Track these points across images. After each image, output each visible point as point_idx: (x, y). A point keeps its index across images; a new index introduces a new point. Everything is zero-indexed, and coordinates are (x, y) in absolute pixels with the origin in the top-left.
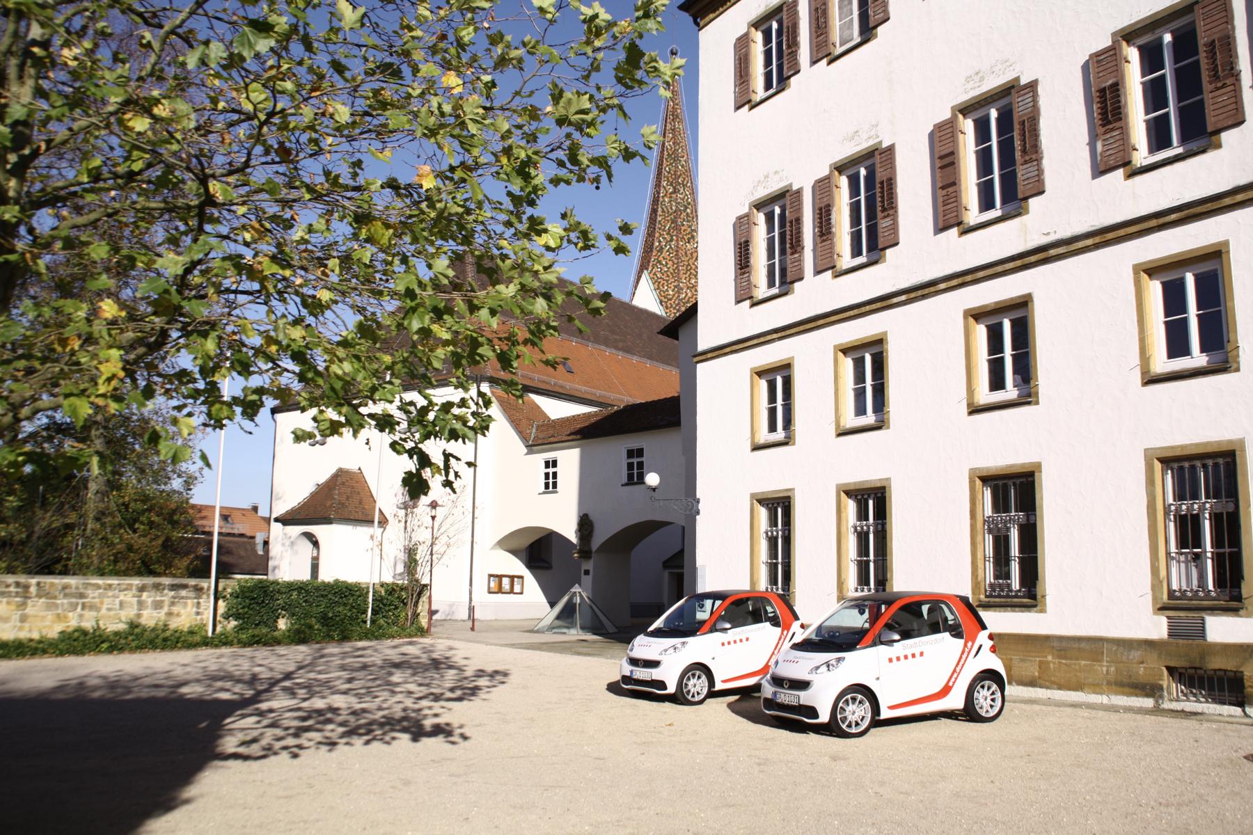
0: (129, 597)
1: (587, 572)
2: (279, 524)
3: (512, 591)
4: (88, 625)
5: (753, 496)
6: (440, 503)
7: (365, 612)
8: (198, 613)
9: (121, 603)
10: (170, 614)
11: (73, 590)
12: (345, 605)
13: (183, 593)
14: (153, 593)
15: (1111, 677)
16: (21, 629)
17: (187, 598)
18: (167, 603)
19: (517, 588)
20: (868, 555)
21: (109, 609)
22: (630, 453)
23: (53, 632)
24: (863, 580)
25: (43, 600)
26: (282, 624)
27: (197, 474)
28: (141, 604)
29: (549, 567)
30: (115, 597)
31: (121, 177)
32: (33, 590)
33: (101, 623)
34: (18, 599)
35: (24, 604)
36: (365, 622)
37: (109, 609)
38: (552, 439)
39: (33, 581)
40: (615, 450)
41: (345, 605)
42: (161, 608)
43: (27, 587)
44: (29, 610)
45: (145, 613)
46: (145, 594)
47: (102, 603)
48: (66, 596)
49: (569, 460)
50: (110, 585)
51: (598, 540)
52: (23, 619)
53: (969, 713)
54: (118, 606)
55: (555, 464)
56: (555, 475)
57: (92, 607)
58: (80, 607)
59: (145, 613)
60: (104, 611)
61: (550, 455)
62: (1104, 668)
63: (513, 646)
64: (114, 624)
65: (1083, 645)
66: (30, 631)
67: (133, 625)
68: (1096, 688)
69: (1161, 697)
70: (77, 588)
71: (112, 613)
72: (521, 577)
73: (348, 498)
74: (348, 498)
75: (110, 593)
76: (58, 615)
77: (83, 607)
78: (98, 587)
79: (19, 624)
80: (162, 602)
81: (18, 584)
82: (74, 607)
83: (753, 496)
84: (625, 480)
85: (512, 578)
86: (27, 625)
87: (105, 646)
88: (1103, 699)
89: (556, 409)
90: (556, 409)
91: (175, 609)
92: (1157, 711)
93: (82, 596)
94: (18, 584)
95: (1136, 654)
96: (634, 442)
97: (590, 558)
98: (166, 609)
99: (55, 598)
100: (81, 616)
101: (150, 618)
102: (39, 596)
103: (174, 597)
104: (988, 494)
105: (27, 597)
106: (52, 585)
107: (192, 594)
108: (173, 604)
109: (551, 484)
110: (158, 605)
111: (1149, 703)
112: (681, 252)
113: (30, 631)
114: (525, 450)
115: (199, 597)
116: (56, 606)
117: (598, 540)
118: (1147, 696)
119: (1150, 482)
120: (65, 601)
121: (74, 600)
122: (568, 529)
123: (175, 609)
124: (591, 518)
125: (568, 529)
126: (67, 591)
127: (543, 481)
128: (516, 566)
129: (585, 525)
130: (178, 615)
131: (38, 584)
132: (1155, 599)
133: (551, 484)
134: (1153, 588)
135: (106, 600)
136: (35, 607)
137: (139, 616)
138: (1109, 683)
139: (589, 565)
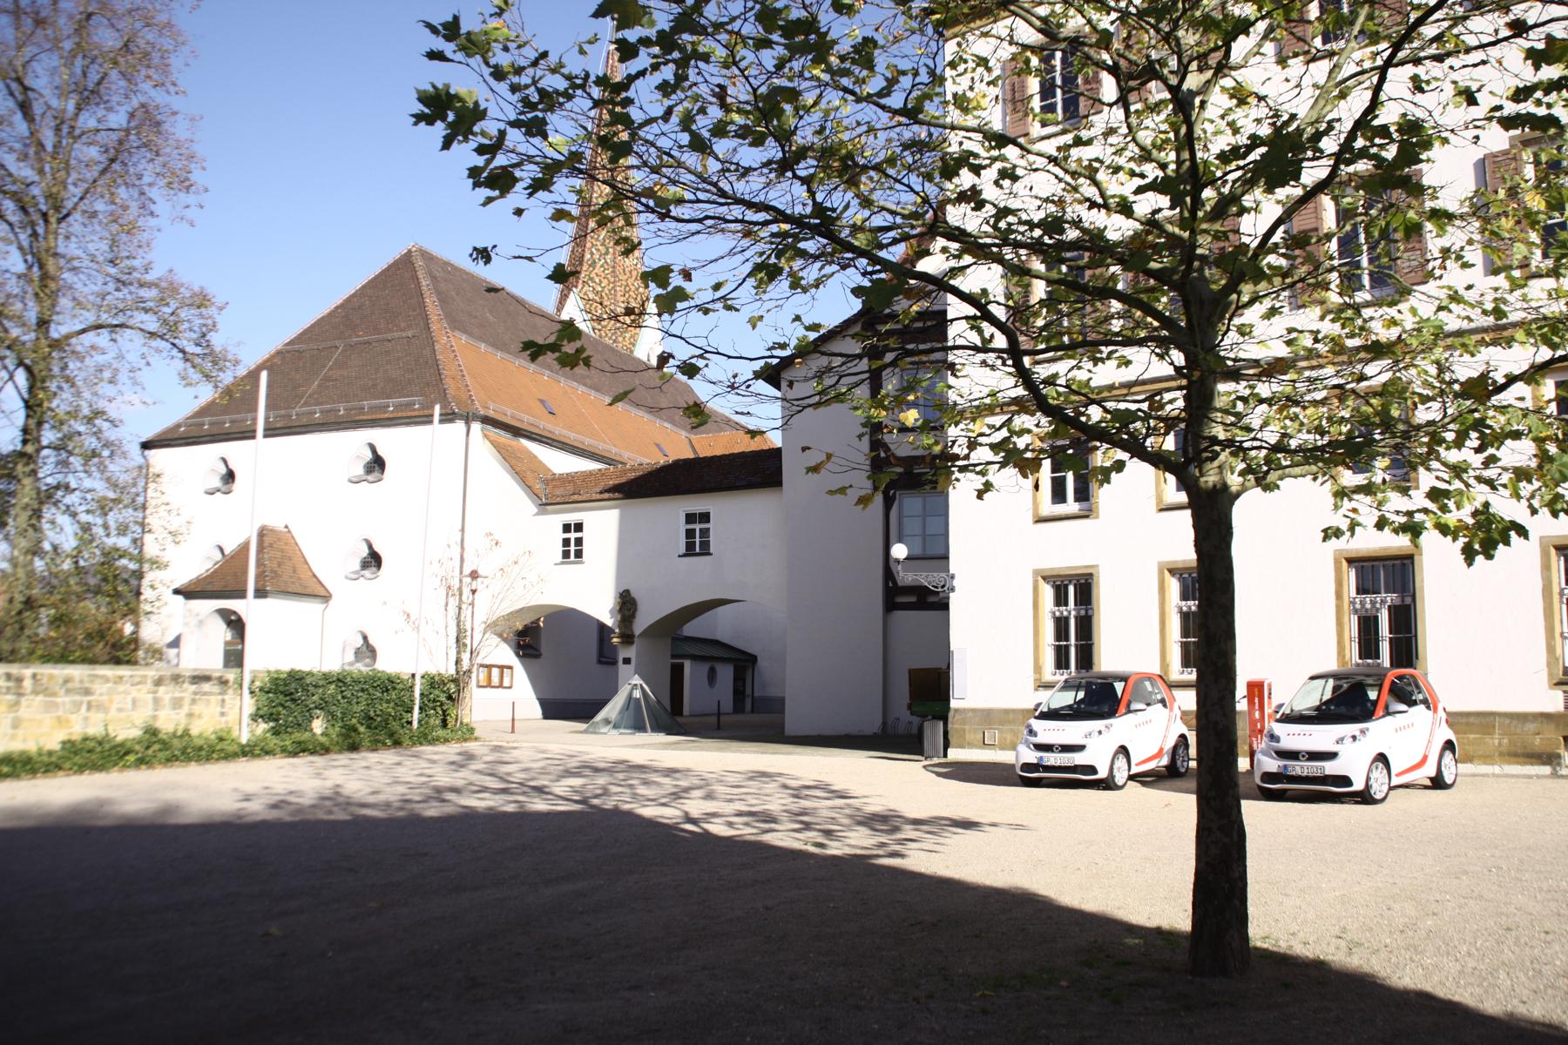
0: (143, 693)
1: (627, 661)
2: (180, 598)
3: (501, 686)
4: (95, 730)
5: (1036, 572)
6: (480, 572)
7: (410, 711)
8: (223, 714)
9: (134, 701)
10: (190, 715)
11: (77, 685)
12: (388, 702)
13: (206, 687)
14: (171, 687)
15: (1504, 749)
16: (13, 737)
17: (210, 694)
18: (187, 701)
19: (506, 683)
20: (1067, 639)
21: (120, 710)
22: (690, 518)
23: (53, 742)
24: (1061, 662)
25: (40, 698)
26: (318, 726)
27: (183, 530)
28: (157, 702)
29: (537, 656)
30: (127, 693)
31: (1038, 226)
32: (28, 684)
33: (110, 729)
34: (9, 697)
35: (17, 703)
36: (410, 723)
37: (120, 710)
38: (576, 497)
39: (27, 672)
40: (670, 514)
41: (388, 702)
42: (180, 707)
43: (19, 680)
44: (23, 712)
45: (162, 714)
46: (162, 689)
47: (111, 701)
48: (68, 691)
49: (603, 525)
50: (121, 678)
51: (645, 619)
52: (16, 724)
53: (1438, 783)
54: (130, 706)
55: (579, 527)
56: (579, 542)
57: (100, 707)
58: (84, 707)
59: (162, 714)
60: (113, 712)
61: (572, 518)
62: (1496, 740)
63: (637, 746)
64: (127, 731)
65: (1472, 720)
66: (24, 740)
67: (152, 732)
68: (1487, 759)
69: (1559, 764)
70: (81, 681)
71: (123, 715)
72: (510, 668)
73: (279, 565)
74: (279, 565)
75: (121, 688)
76: (59, 718)
77: (89, 707)
78: (106, 679)
79: (10, 731)
80: (181, 699)
81: (9, 677)
82: (77, 706)
83: (1036, 572)
84: (683, 550)
85: (502, 668)
86: (20, 732)
87: (131, 758)
88: (1497, 769)
89: (561, 463)
90: (561, 463)
91: (197, 709)
92: (1555, 775)
93: (87, 692)
94: (9, 677)
95: (1531, 727)
96: (697, 504)
97: (632, 643)
98: (186, 709)
99: (54, 694)
100: (86, 719)
101: (168, 722)
102: (35, 692)
103: (195, 693)
104: (1353, 574)
105: (20, 695)
106: (51, 677)
107: (216, 689)
108: (194, 701)
109: (573, 550)
110: (177, 704)
111: (1547, 770)
112: (619, 269)
113: (24, 740)
114: (536, 510)
115: (223, 693)
116: (56, 705)
117: (641, 623)
118: (1544, 763)
119: (1546, 567)
120: (67, 699)
121: (78, 698)
122: (603, 609)
123: (197, 709)
124: (634, 594)
125: (603, 609)
126: (70, 685)
127: (560, 549)
128: (505, 654)
129: (627, 604)
130: (200, 716)
131: (34, 676)
132: (1550, 675)
133: (573, 550)
134: (1549, 664)
135: (117, 698)
136: (32, 706)
137: (155, 717)
138: (1501, 754)
139: (631, 652)
